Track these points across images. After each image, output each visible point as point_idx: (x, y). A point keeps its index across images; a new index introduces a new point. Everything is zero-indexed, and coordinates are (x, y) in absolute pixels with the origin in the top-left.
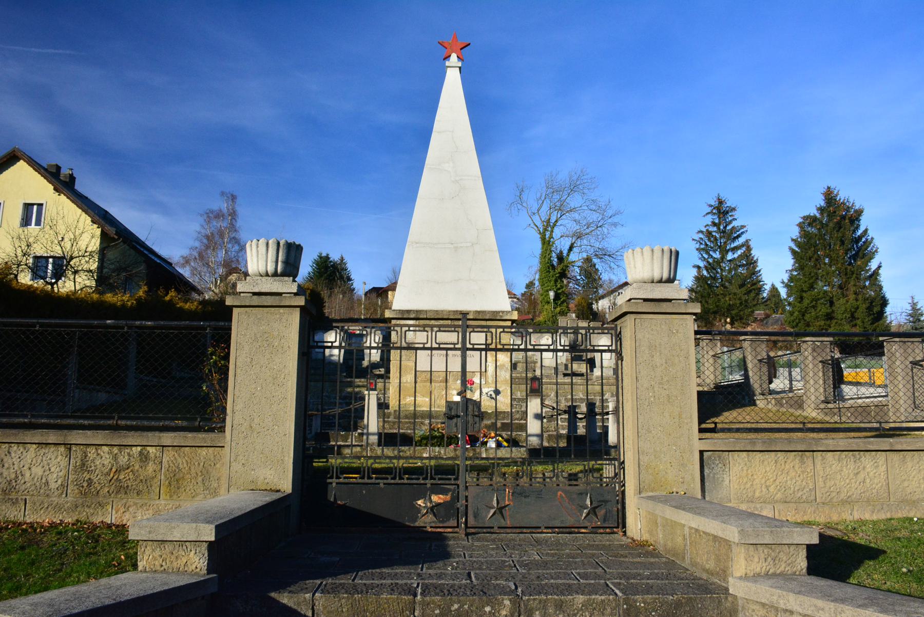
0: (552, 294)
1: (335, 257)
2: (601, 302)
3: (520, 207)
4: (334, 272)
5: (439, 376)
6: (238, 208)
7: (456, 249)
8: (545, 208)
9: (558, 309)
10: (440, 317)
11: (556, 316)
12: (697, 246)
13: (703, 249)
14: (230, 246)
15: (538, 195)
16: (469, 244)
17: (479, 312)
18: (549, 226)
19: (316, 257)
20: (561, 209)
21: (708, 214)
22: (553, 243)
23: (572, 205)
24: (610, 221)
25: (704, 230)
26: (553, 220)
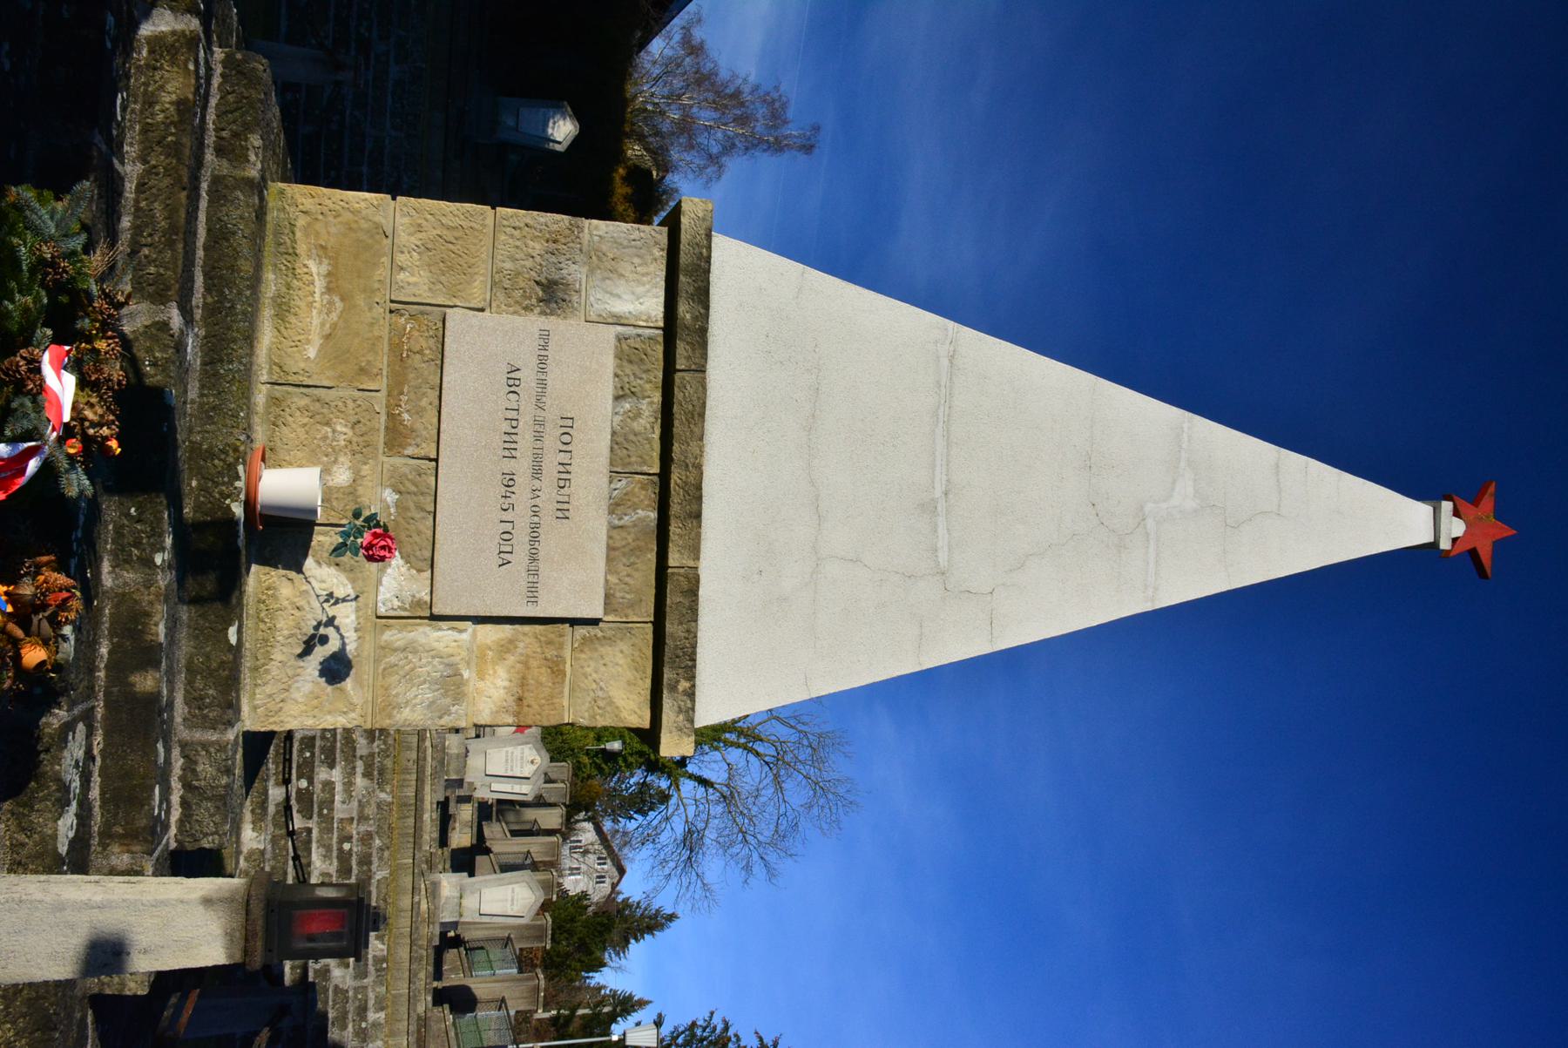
0: (616, 746)
2: (589, 826)
5: (419, 412)
6: (786, 155)
7: (928, 508)
9: (585, 760)
10: (678, 428)
11: (574, 755)
13: (693, 1035)
14: (719, 135)
15: (805, 719)
16: (943, 557)
17: (692, 591)
20: (778, 764)
21: (761, 1039)
22: (717, 749)
23: (788, 785)
24: (755, 856)
25: (731, 1033)
26: (758, 747)
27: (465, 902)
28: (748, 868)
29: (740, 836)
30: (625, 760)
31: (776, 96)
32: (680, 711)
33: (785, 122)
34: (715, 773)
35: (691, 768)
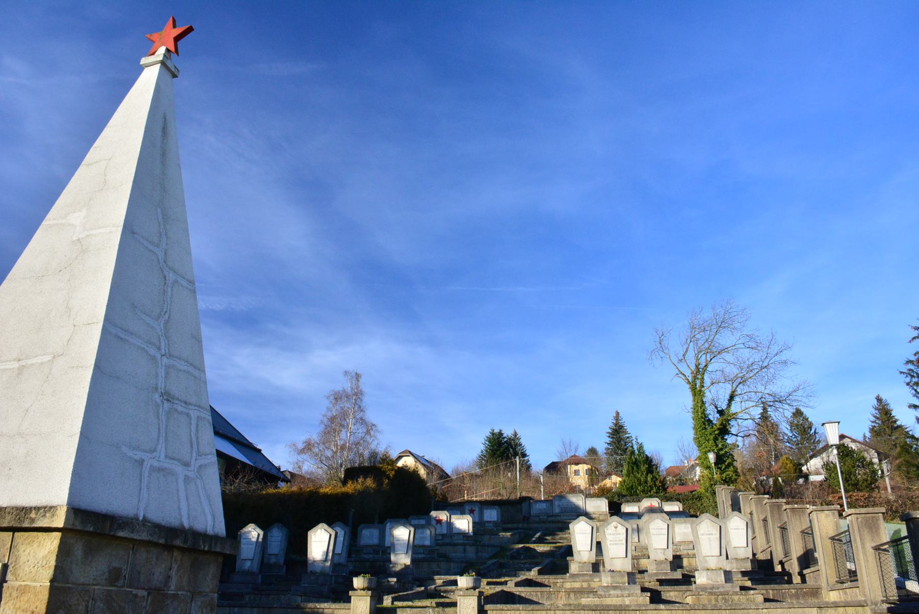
0: (712, 457)
1: (508, 433)
3: (662, 354)
4: (507, 448)
8: (691, 355)
12: (908, 380)
18: (699, 372)
19: (488, 434)
20: (715, 352)
21: (914, 338)
25: (913, 358)
27: (713, 566)
28: (785, 363)
29: (765, 370)
30: (721, 449)
31: (332, 398)
32: (44, 516)
33: (344, 391)
34: (724, 392)
35: (724, 407)
